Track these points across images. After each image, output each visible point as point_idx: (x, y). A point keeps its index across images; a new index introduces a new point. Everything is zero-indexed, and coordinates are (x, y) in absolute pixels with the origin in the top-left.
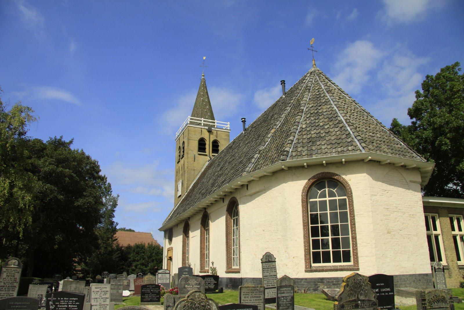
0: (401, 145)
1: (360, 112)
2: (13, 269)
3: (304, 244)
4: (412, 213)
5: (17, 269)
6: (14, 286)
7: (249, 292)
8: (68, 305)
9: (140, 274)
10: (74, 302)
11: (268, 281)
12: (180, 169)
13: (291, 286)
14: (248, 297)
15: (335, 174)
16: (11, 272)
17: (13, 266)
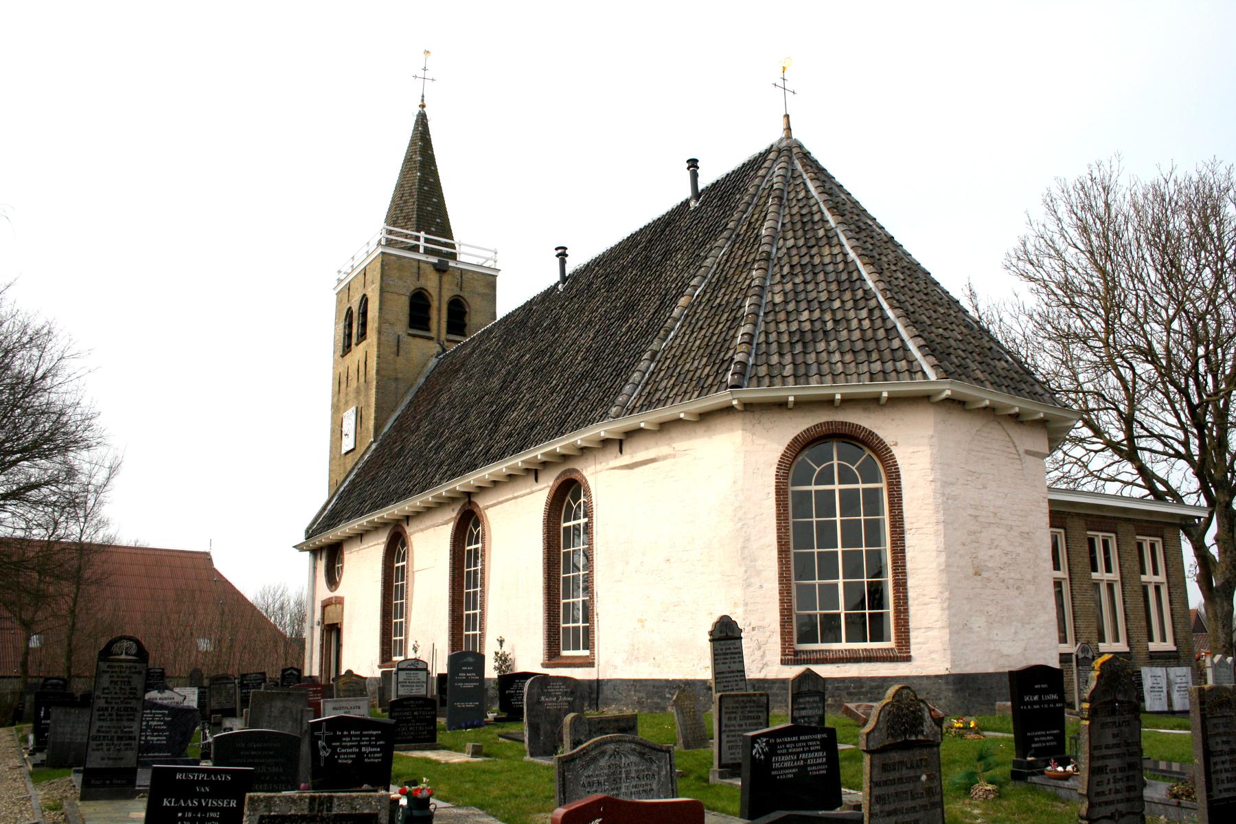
0: (1007, 361)
2: (124, 664)
3: (780, 596)
4: (1026, 529)
5: (136, 665)
6: (132, 708)
7: (737, 707)
8: (359, 747)
9: (292, 674)
10: (373, 741)
11: (726, 684)
12: (353, 374)
13: (820, 692)
14: (735, 718)
15: (860, 426)
16: (121, 672)
17: (123, 657)
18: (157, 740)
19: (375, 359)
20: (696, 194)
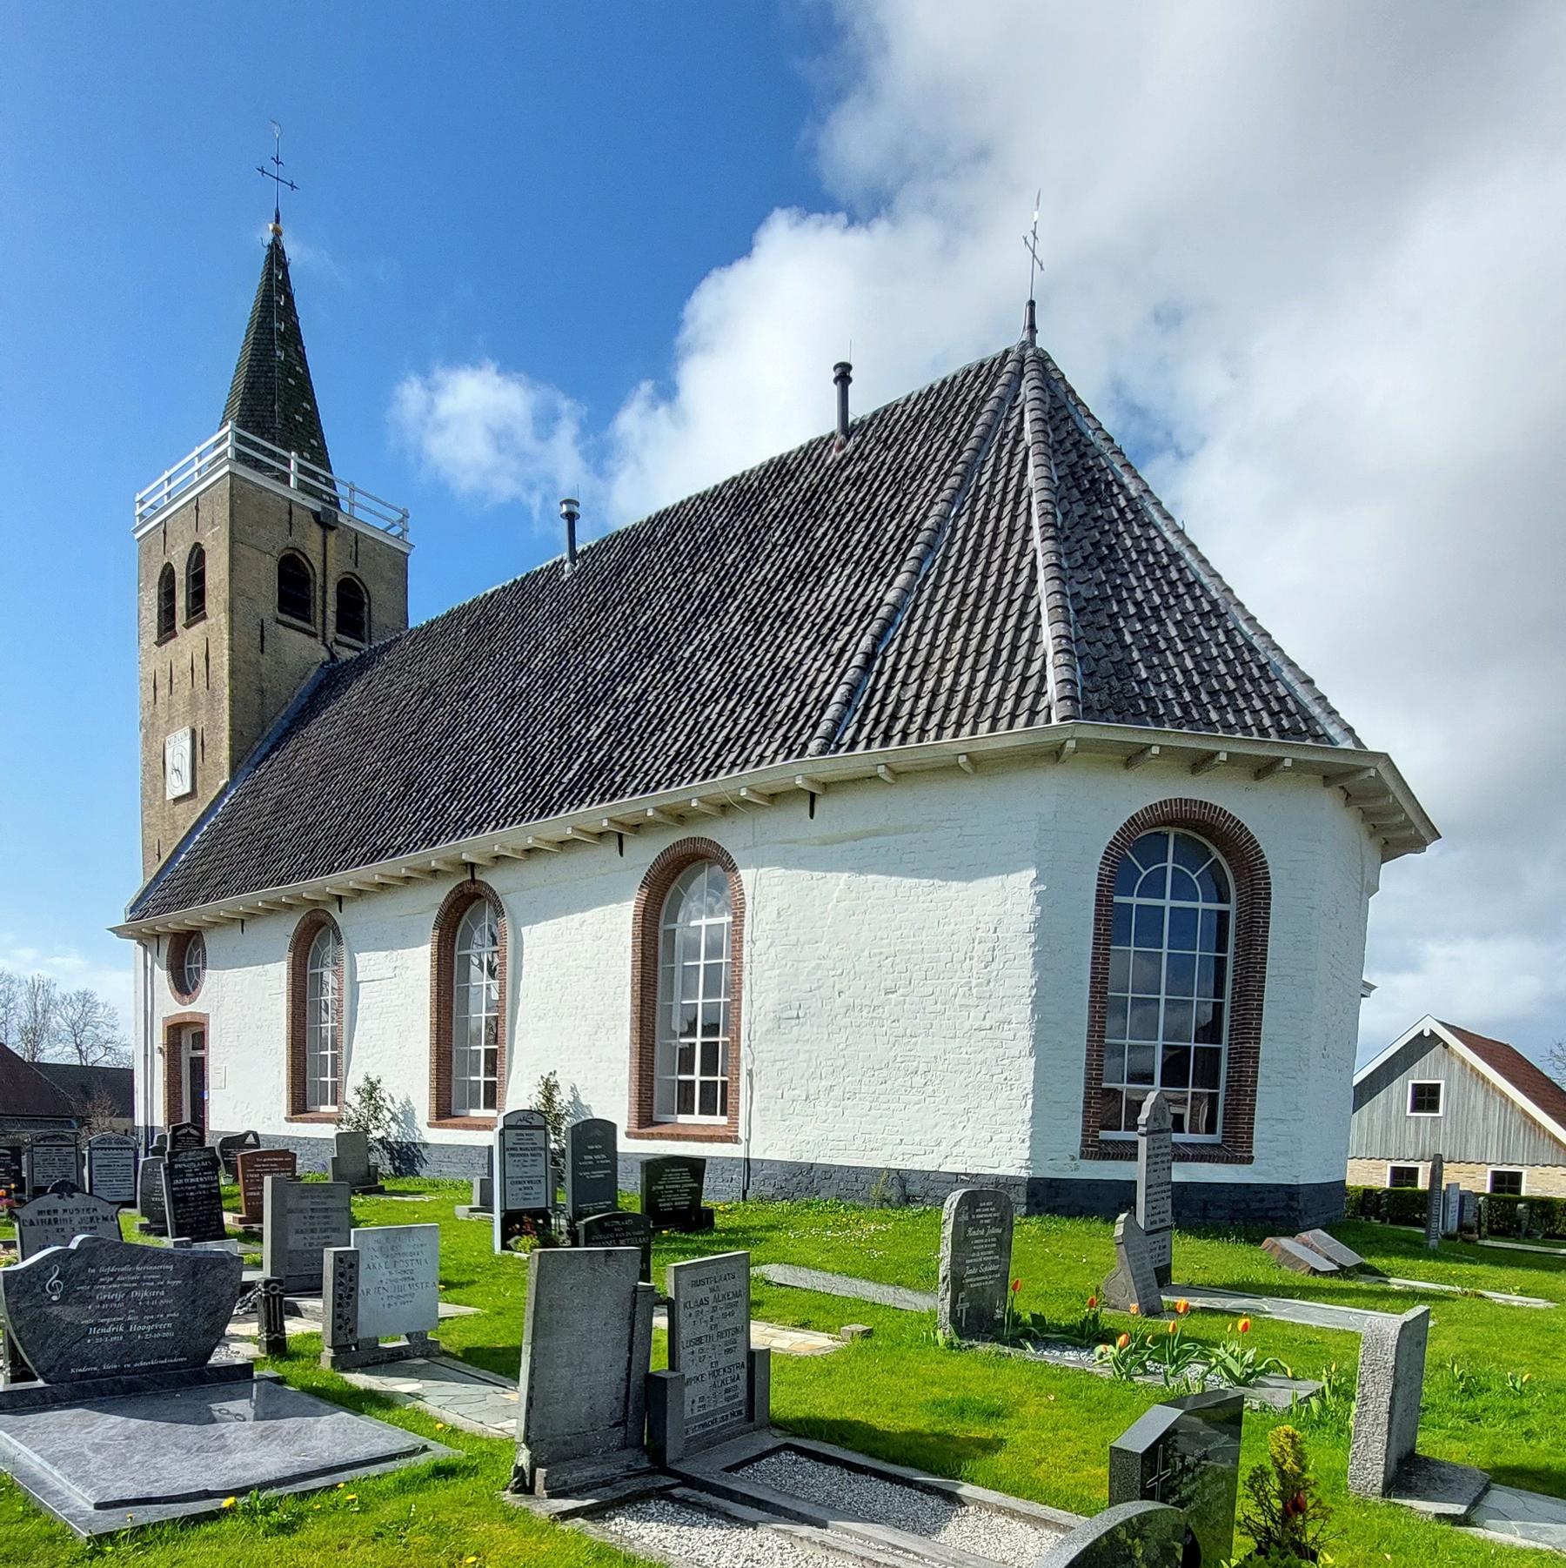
1: (1098, 629)
9: (189, 1134)
18: (154, 1331)
19: (226, 652)
20: (847, 430)
